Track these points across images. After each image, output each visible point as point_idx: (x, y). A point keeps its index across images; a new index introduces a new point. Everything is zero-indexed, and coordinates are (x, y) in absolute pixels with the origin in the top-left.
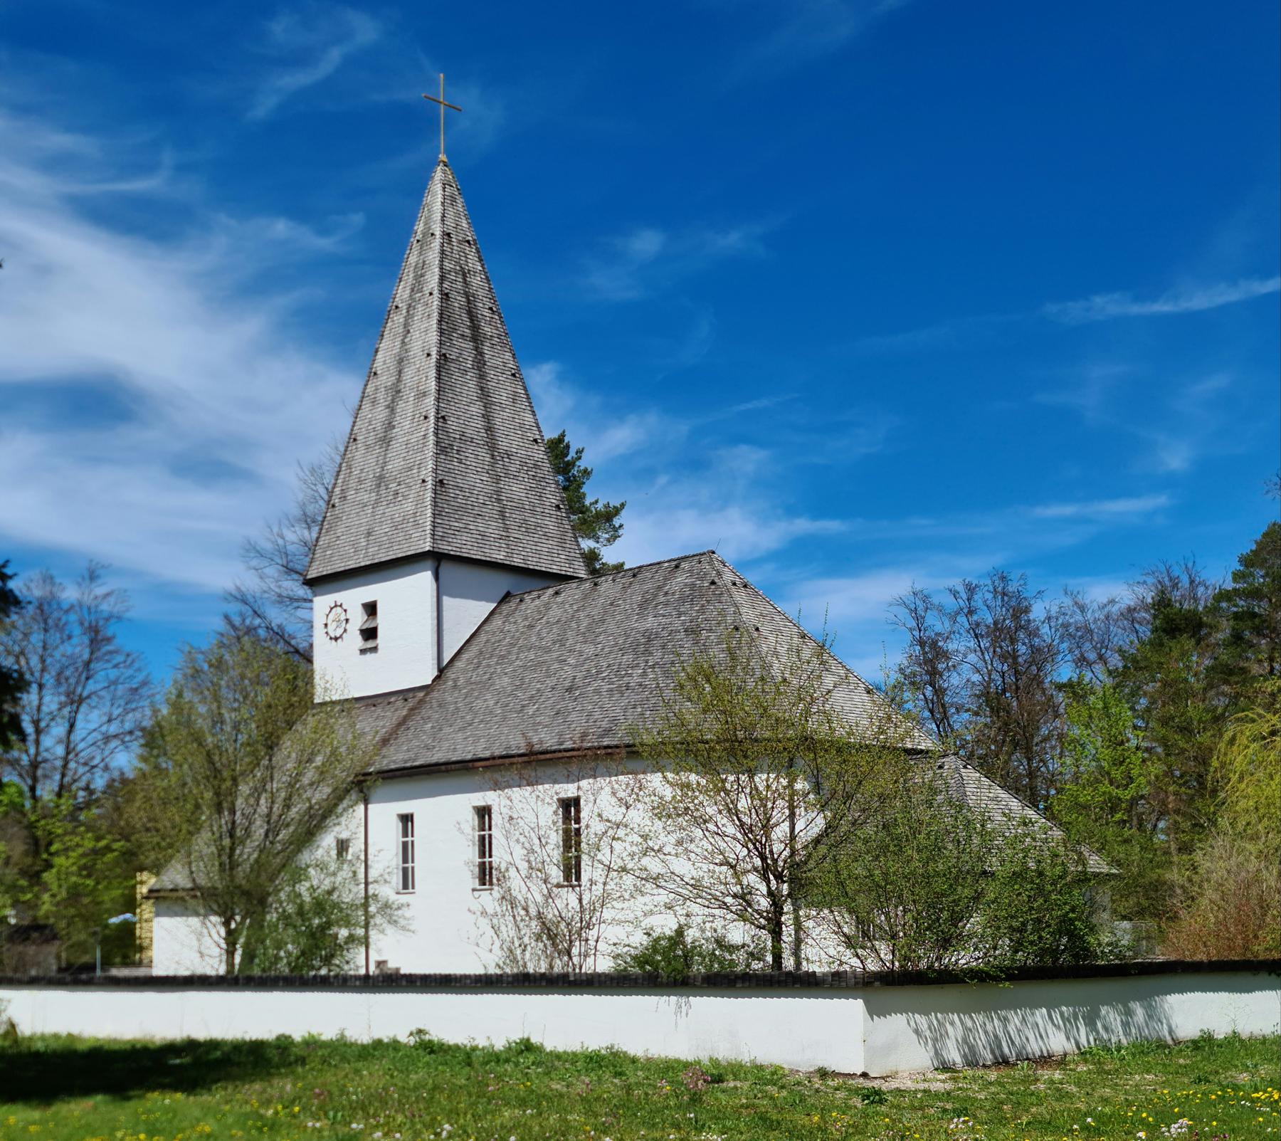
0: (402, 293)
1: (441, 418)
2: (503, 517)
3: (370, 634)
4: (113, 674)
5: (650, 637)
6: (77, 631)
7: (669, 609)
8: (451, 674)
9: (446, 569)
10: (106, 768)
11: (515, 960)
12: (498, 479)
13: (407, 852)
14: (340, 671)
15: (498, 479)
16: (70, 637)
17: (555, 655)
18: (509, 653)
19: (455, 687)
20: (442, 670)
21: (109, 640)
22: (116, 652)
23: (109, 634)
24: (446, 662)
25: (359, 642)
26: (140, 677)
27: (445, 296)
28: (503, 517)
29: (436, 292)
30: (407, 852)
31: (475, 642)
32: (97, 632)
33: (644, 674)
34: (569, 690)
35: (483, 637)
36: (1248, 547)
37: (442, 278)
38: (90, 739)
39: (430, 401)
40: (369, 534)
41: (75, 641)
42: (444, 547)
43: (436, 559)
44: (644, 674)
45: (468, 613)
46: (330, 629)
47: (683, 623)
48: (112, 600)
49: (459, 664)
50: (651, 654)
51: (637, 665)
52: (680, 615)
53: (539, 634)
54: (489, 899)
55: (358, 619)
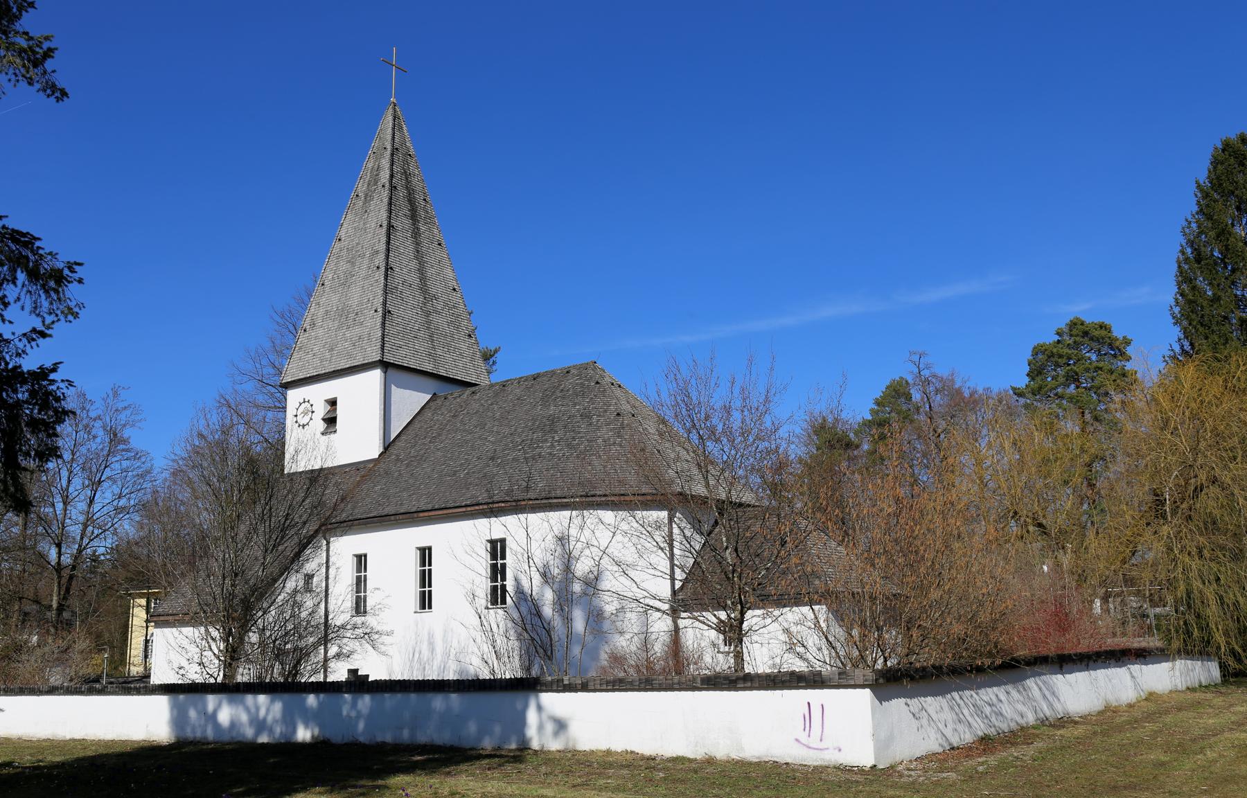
0: (361, 187)
1: (388, 268)
2: (433, 341)
3: (331, 421)
4: (125, 464)
5: (553, 420)
6: (101, 433)
7: (566, 402)
8: (391, 450)
9: (391, 371)
10: (115, 533)
11: (1044, 683)
12: (428, 314)
13: (360, 583)
14: (307, 449)
15: (428, 314)
16: (95, 437)
17: (476, 436)
18: (439, 435)
19: (398, 460)
20: (387, 447)
21: (125, 441)
22: (127, 450)
23: (126, 436)
24: (393, 436)
25: (322, 426)
26: (145, 467)
27: (393, 188)
28: (433, 341)
29: (387, 185)
30: (360, 583)
31: (411, 428)
32: (115, 435)
33: (552, 446)
34: (492, 459)
35: (417, 425)
36: (878, 394)
37: (392, 176)
38: (105, 510)
39: (382, 256)
40: (332, 350)
41: (98, 440)
42: (389, 358)
43: (385, 365)
44: (552, 446)
45: (410, 401)
46: (299, 418)
47: (578, 411)
48: (128, 412)
49: (398, 443)
50: (556, 432)
51: (546, 440)
52: (575, 405)
53: (462, 421)
54: (497, 617)
55: (321, 410)
